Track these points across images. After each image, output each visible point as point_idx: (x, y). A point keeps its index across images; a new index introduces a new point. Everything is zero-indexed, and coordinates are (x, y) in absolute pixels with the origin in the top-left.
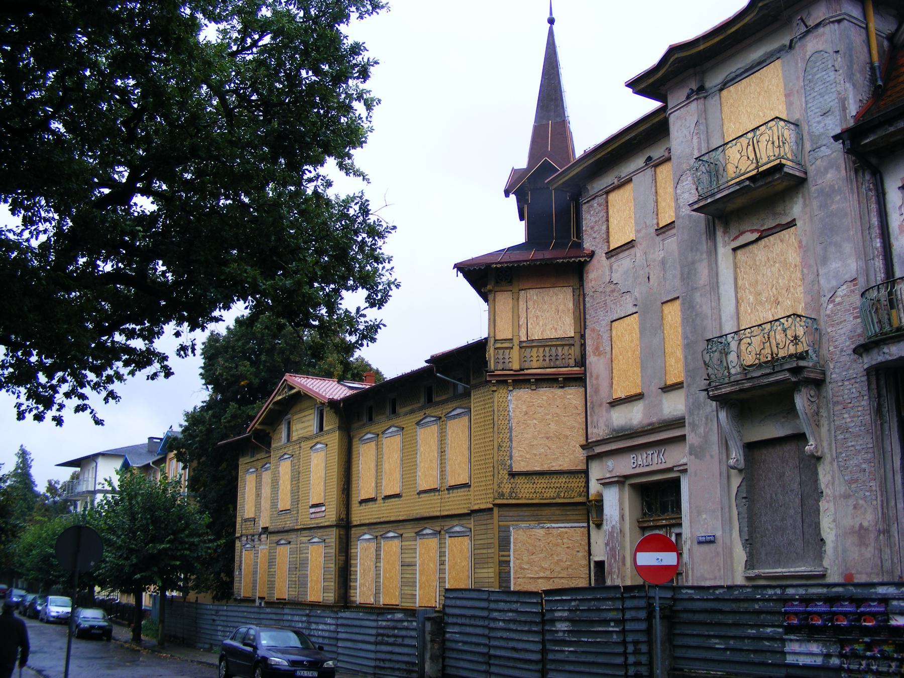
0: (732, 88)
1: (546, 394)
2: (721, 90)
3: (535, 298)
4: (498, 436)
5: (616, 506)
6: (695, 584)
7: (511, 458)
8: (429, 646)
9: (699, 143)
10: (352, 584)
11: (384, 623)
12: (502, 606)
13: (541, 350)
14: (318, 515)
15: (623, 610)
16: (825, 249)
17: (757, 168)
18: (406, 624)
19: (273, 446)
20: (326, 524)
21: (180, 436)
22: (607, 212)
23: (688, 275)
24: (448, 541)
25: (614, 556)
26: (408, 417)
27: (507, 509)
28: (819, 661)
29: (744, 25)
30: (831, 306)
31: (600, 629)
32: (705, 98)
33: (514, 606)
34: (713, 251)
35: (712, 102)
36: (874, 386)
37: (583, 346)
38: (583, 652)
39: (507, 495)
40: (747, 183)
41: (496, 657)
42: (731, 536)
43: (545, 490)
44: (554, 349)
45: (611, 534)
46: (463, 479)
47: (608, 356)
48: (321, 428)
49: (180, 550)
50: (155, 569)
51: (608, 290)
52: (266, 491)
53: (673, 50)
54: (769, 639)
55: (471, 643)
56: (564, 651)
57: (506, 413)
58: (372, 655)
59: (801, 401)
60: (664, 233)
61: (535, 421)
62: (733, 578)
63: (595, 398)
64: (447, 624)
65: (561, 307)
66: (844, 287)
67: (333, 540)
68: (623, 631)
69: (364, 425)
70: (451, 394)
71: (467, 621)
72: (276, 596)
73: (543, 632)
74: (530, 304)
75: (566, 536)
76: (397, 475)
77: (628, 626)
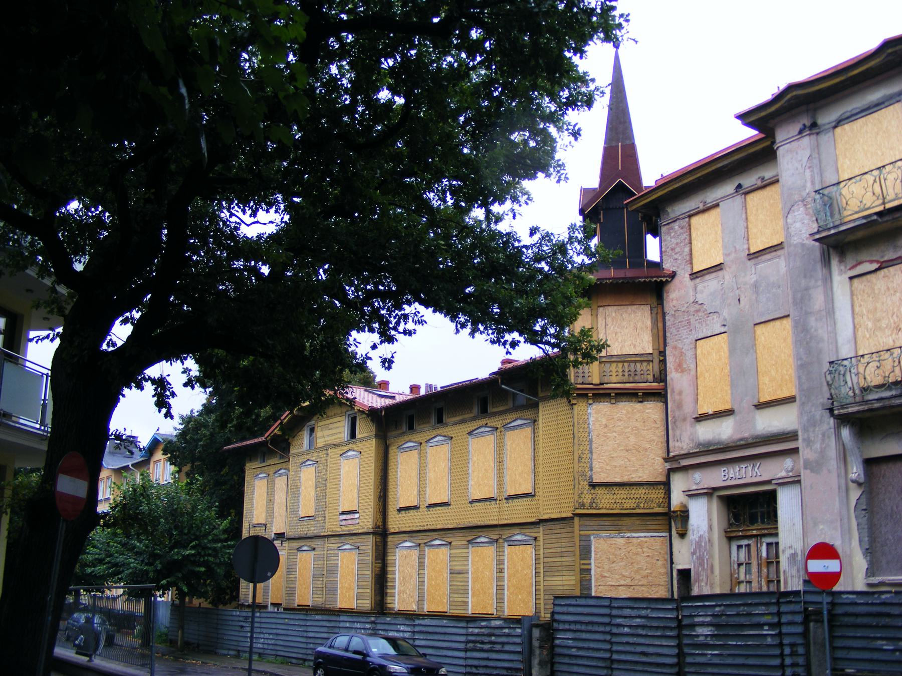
0: (847, 127)
1: (625, 408)
2: (835, 127)
3: (614, 314)
4: (579, 446)
5: (703, 517)
7: (591, 469)
8: (537, 652)
9: (813, 177)
10: (389, 591)
11: (476, 631)
12: (627, 612)
13: (620, 365)
14: (350, 522)
15: (779, 614)
17: (884, 203)
18: (506, 631)
19: (293, 451)
20: (360, 531)
21: (175, 439)
22: (690, 235)
23: (801, 299)
24: (507, 549)
26: (457, 427)
29: (867, 70)
31: (751, 633)
32: (818, 134)
33: (643, 612)
34: (828, 279)
35: (825, 138)
37: (663, 362)
38: (729, 655)
39: (587, 505)
40: (875, 217)
41: (619, 661)
42: (850, 544)
43: (625, 501)
44: (632, 365)
45: (698, 544)
46: (526, 487)
47: (693, 372)
48: (353, 435)
49: (203, 556)
50: (180, 575)
51: (692, 309)
52: (280, 496)
53: (791, 88)
55: (588, 649)
56: (706, 655)
57: (586, 426)
58: (462, 662)
60: (757, 257)
61: (615, 434)
62: (853, 585)
63: (677, 413)
64: (558, 630)
65: (639, 325)
67: (370, 547)
68: (780, 634)
69: (403, 433)
70: (510, 405)
71: (583, 627)
72: (296, 603)
73: (678, 637)
74: (609, 320)
75: (646, 545)
76: (445, 483)
77: (785, 630)
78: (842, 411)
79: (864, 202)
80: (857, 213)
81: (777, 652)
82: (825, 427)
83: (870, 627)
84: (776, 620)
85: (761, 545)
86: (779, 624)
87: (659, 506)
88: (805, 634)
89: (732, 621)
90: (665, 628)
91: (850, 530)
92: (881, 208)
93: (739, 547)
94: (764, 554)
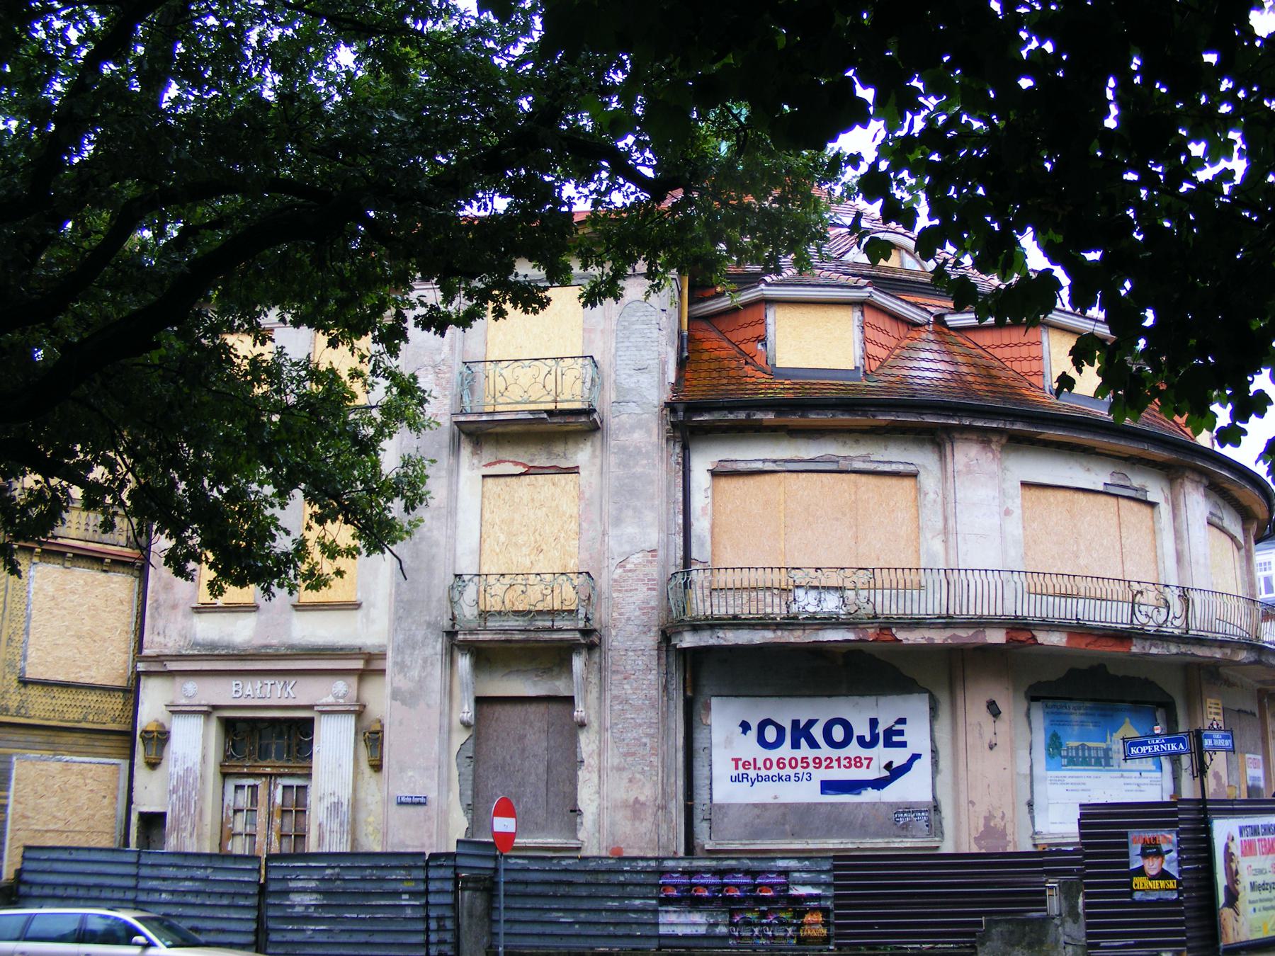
5: (193, 745)
6: (389, 850)
7: (25, 658)
15: (427, 880)
16: (620, 510)
25: (186, 807)
27: (11, 730)
28: (702, 930)
30: (620, 571)
31: (383, 903)
33: (200, 873)
34: (454, 472)
36: (663, 661)
38: (342, 931)
39: (12, 710)
40: (545, 416)
43: (66, 709)
45: (183, 780)
54: (636, 911)
56: (303, 930)
57: (24, 594)
59: (578, 663)
61: (65, 612)
63: (162, 597)
66: (641, 555)
73: (258, 907)
78: (469, 637)
79: (530, 393)
80: (518, 403)
81: (422, 926)
82: (429, 651)
83: (546, 896)
84: (422, 887)
85: (276, 787)
86: (427, 892)
87: (114, 721)
88: (454, 906)
89: (351, 887)
90: (234, 895)
91: (449, 779)
92: (551, 406)
93: (238, 788)
94: (279, 800)
